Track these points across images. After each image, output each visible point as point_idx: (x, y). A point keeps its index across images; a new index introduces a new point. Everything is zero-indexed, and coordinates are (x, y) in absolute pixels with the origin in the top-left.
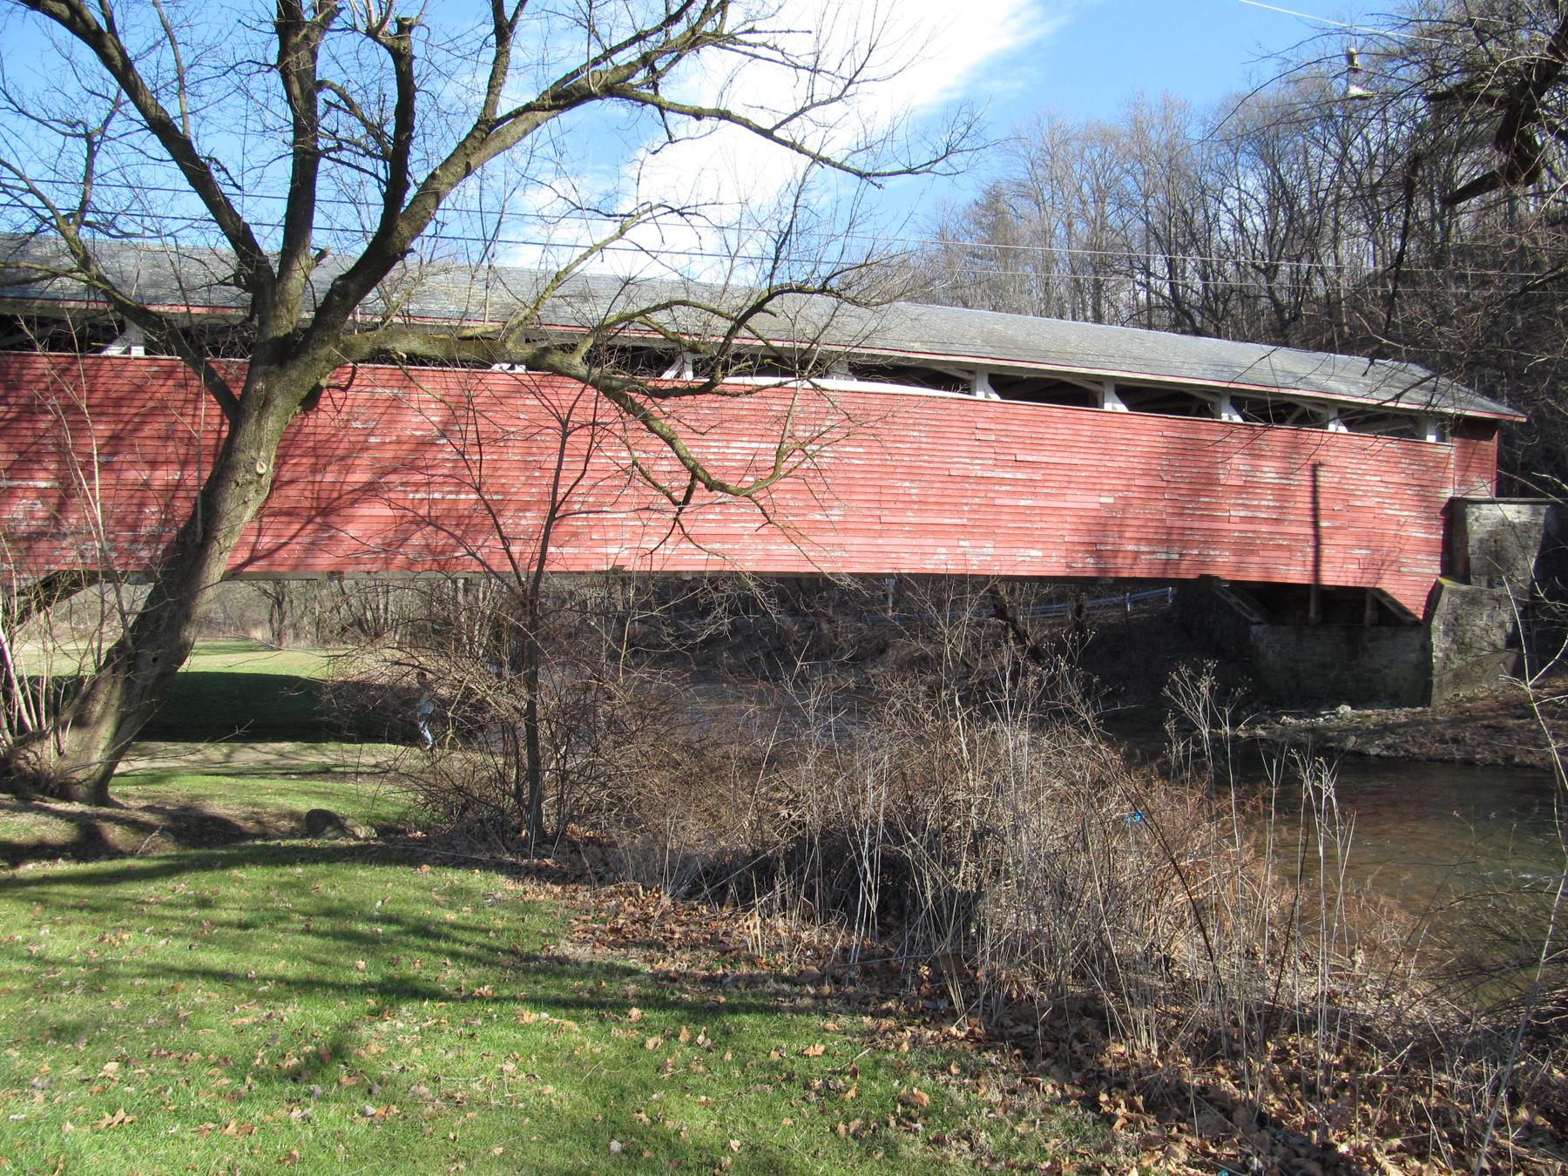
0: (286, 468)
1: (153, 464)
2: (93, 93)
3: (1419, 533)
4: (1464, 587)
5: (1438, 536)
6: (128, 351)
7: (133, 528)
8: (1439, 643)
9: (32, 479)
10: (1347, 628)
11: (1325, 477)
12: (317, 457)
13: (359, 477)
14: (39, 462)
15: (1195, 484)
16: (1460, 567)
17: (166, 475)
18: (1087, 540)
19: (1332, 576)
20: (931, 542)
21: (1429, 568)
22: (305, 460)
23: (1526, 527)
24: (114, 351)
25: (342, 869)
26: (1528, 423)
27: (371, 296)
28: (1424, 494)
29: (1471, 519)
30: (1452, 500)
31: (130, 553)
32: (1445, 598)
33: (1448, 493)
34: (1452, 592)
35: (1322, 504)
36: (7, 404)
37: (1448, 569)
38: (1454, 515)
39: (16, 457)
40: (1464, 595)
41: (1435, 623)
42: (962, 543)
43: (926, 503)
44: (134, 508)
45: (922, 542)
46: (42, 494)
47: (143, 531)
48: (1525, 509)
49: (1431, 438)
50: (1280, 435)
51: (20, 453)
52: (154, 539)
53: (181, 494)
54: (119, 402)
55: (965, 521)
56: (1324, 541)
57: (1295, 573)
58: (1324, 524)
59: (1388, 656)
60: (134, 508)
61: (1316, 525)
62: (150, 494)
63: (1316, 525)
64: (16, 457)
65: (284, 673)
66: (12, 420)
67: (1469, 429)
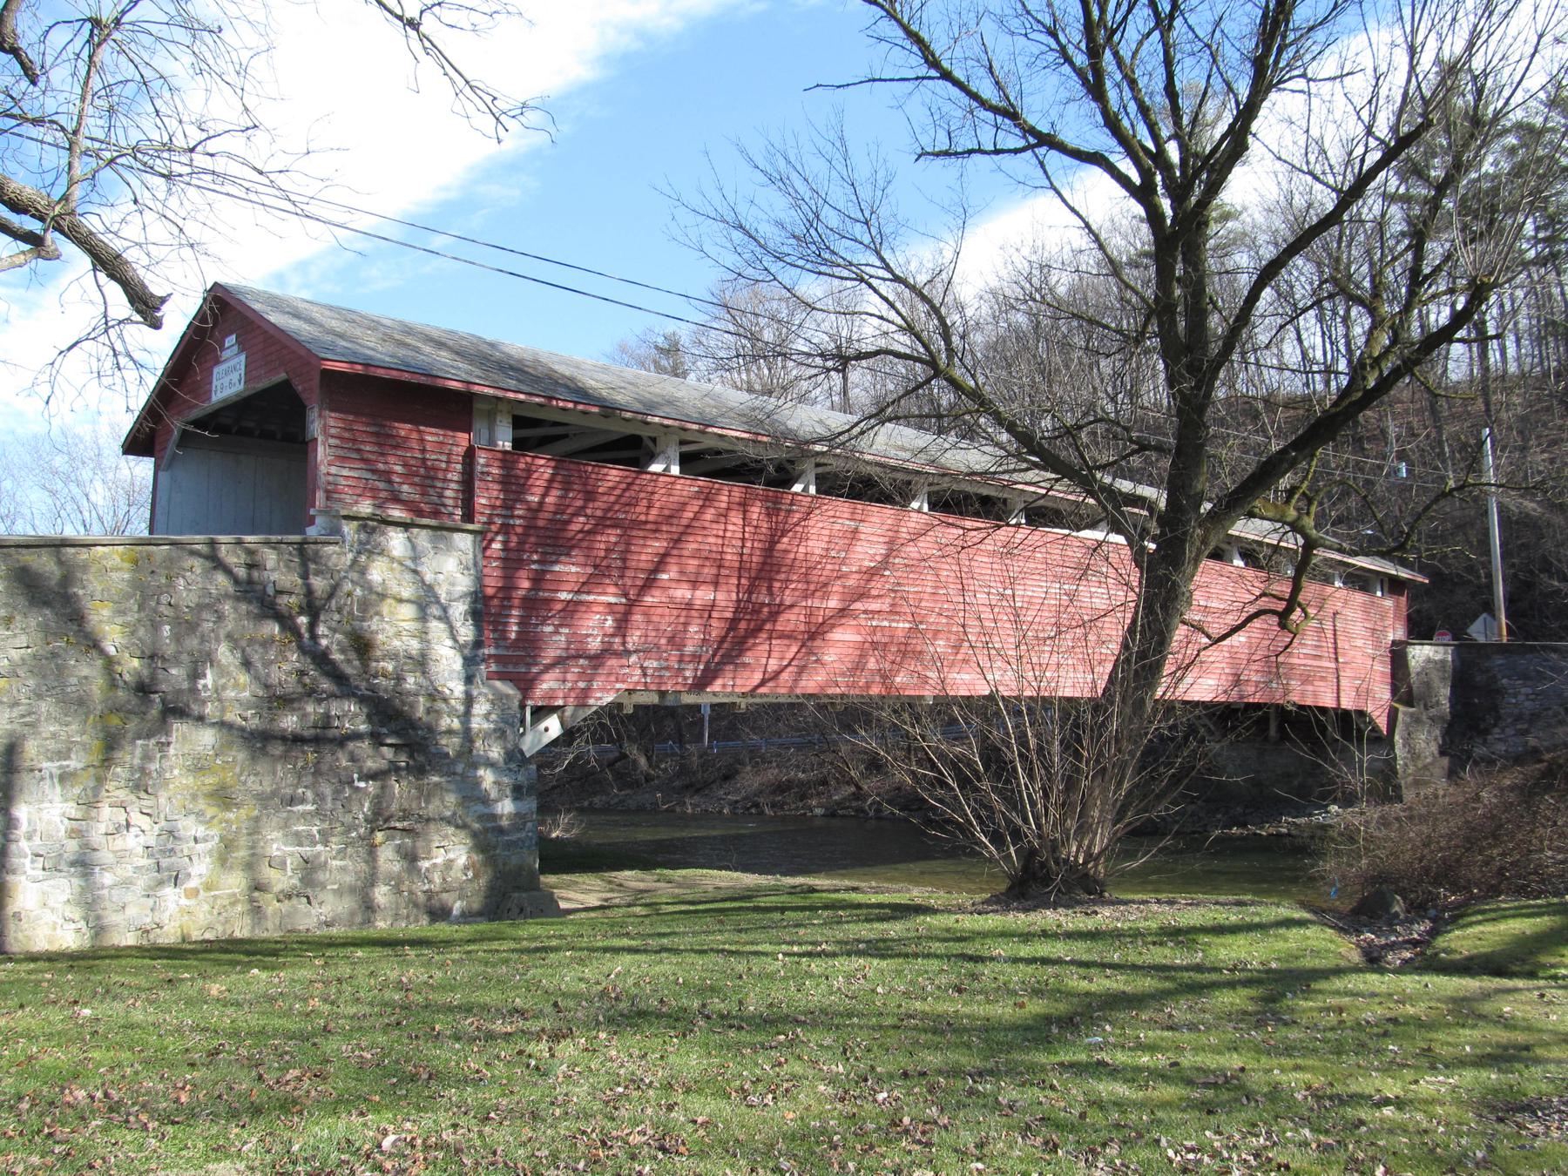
0: (787, 592)
1: (695, 584)
2: (1279, 159)
5: (1388, 670)
7: (680, 647)
8: (1400, 750)
9: (605, 594)
10: (1288, 744)
12: (808, 583)
13: (833, 603)
19: (1346, 704)
21: (1383, 693)
23: (1443, 662)
25: (1228, 939)
32: (1400, 716)
33: (1391, 637)
34: (1405, 713)
37: (1394, 691)
38: (1398, 657)
39: (590, 570)
40: (1412, 715)
41: (1397, 737)
44: (681, 628)
49: (1379, 594)
51: (596, 567)
52: (696, 658)
57: (1328, 701)
59: (1357, 769)
60: (681, 628)
62: (694, 613)
64: (590, 570)
66: (589, 532)
67: (1394, 586)
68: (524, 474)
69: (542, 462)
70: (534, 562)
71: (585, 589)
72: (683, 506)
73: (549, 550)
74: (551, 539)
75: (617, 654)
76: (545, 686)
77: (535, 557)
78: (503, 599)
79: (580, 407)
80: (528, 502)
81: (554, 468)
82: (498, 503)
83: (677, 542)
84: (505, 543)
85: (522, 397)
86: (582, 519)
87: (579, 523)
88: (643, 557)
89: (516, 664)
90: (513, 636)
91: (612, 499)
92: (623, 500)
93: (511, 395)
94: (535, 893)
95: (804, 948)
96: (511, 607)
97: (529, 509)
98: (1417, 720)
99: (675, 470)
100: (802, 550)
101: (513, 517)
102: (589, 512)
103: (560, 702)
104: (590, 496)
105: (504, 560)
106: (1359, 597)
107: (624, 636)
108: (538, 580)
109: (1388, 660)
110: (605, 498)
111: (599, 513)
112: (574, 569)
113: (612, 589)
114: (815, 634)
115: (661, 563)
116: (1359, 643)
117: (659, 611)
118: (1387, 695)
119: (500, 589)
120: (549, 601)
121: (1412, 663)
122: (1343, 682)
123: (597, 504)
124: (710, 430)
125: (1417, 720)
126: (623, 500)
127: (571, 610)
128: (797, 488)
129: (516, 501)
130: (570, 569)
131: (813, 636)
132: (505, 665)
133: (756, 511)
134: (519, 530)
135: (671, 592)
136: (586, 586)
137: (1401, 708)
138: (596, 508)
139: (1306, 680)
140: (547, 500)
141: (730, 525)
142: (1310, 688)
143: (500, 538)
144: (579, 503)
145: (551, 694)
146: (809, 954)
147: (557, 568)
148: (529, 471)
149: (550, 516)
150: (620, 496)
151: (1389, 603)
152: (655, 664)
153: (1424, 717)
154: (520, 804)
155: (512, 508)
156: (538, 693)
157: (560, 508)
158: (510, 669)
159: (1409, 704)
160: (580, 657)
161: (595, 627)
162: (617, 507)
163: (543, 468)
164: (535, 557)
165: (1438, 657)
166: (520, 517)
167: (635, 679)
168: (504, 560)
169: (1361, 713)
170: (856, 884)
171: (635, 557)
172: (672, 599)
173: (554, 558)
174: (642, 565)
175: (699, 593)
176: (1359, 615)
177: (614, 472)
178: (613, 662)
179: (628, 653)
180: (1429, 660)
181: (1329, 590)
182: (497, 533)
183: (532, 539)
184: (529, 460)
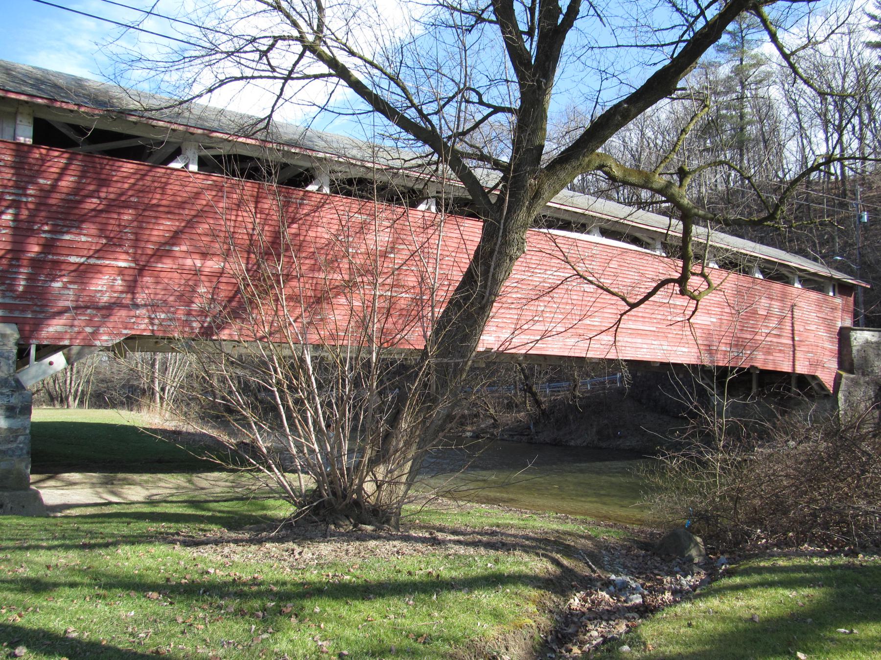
1: (204, 255)
3: (828, 345)
4: (852, 376)
5: (835, 347)
6: (186, 166)
9: (116, 259)
11: (797, 313)
14: (120, 246)
15: (744, 314)
16: (847, 364)
17: (213, 265)
18: (705, 343)
19: (800, 370)
20: (640, 341)
21: (833, 365)
22: (307, 261)
24: (176, 165)
26: (871, 289)
27: (639, 116)
28: (828, 323)
29: (852, 339)
30: (841, 328)
31: (187, 323)
32: (843, 381)
33: (839, 324)
34: (846, 379)
35: (796, 328)
36: (99, 198)
37: (841, 365)
38: (843, 336)
40: (852, 380)
41: (840, 395)
42: (654, 342)
43: (638, 316)
45: (633, 340)
46: (121, 271)
47: (194, 307)
48: (876, 334)
49: (831, 294)
50: (777, 286)
52: (203, 313)
53: (223, 280)
54: (182, 205)
55: (654, 329)
56: (797, 348)
57: (786, 368)
58: (796, 339)
61: (793, 339)
63: (793, 339)
64: (104, 241)
65: (113, 423)
66: (101, 211)
67: (843, 289)
68: (40, 162)
69: (57, 154)
70: (45, 232)
71: (101, 254)
72: (197, 195)
73: (60, 223)
74: (69, 215)
75: (126, 307)
76: (51, 329)
77: (46, 228)
78: (12, 259)
79: (82, 109)
80: (38, 183)
81: (68, 159)
82: (11, 184)
83: (190, 224)
84: (16, 215)
85: (23, 98)
86: (94, 200)
87: (92, 203)
88: (155, 233)
89: (23, 311)
90: (21, 289)
91: (126, 186)
92: (137, 187)
93: (13, 96)
94: (21, 493)
95: (456, 538)
96: (19, 266)
97: (41, 190)
98: (856, 383)
99: (194, 167)
100: (311, 233)
101: (26, 195)
102: (103, 195)
103: (67, 342)
104: (105, 182)
105: (15, 228)
106: (813, 295)
107: (133, 293)
108: (49, 246)
109: (836, 340)
110: (119, 185)
111: (112, 196)
112: (84, 239)
113: (124, 256)
114: (320, 299)
115: (175, 237)
116: (813, 327)
117: (170, 275)
118: (834, 365)
119: (8, 251)
120: (57, 264)
121: (854, 343)
122: (798, 354)
123: (111, 190)
124: (215, 134)
125: (856, 383)
126: (137, 187)
127: (83, 273)
128: (312, 188)
129: (29, 183)
130: (83, 239)
131: (319, 300)
132: (11, 311)
133: (267, 203)
134: (31, 206)
135: (181, 261)
136: (101, 253)
137: (844, 374)
138: (110, 192)
139: (768, 352)
140: (62, 184)
141: (246, 213)
142: (771, 358)
143: (10, 211)
144: (91, 188)
145: (60, 336)
146: (459, 542)
147: (67, 237)
148: (43, 160)
149: (63, 196)
150: (134, 184)
151: (838, 301)
152: (163, 316)
153: (862, 381)
154: (12, 421)
155: (25, 189)
156: (44, 334)
157: (77, 190)
158: (16, 314)
159: (851, 371)
160: (87, 307)
161: (105, 285)
162: (130, 193)
163: (57, 159)
164: (46, 228)
165: (874, 339)
166: (32, 196)
167: (143, 327)
168: (15, 228)
169: (814, 377)
170: (511, 496)
171: (148, 232)
172: (182, 267)
173: (65, 229)
174: (153, 239)
175: (209, 263)
176: (813, 307)
177: (129, 165)
178: (123, 313)
179: (137, 306)
180: (867, 342)
181: (789, 289)
182: (8, 207)
183: (43, 214)
184: (44, 151)
